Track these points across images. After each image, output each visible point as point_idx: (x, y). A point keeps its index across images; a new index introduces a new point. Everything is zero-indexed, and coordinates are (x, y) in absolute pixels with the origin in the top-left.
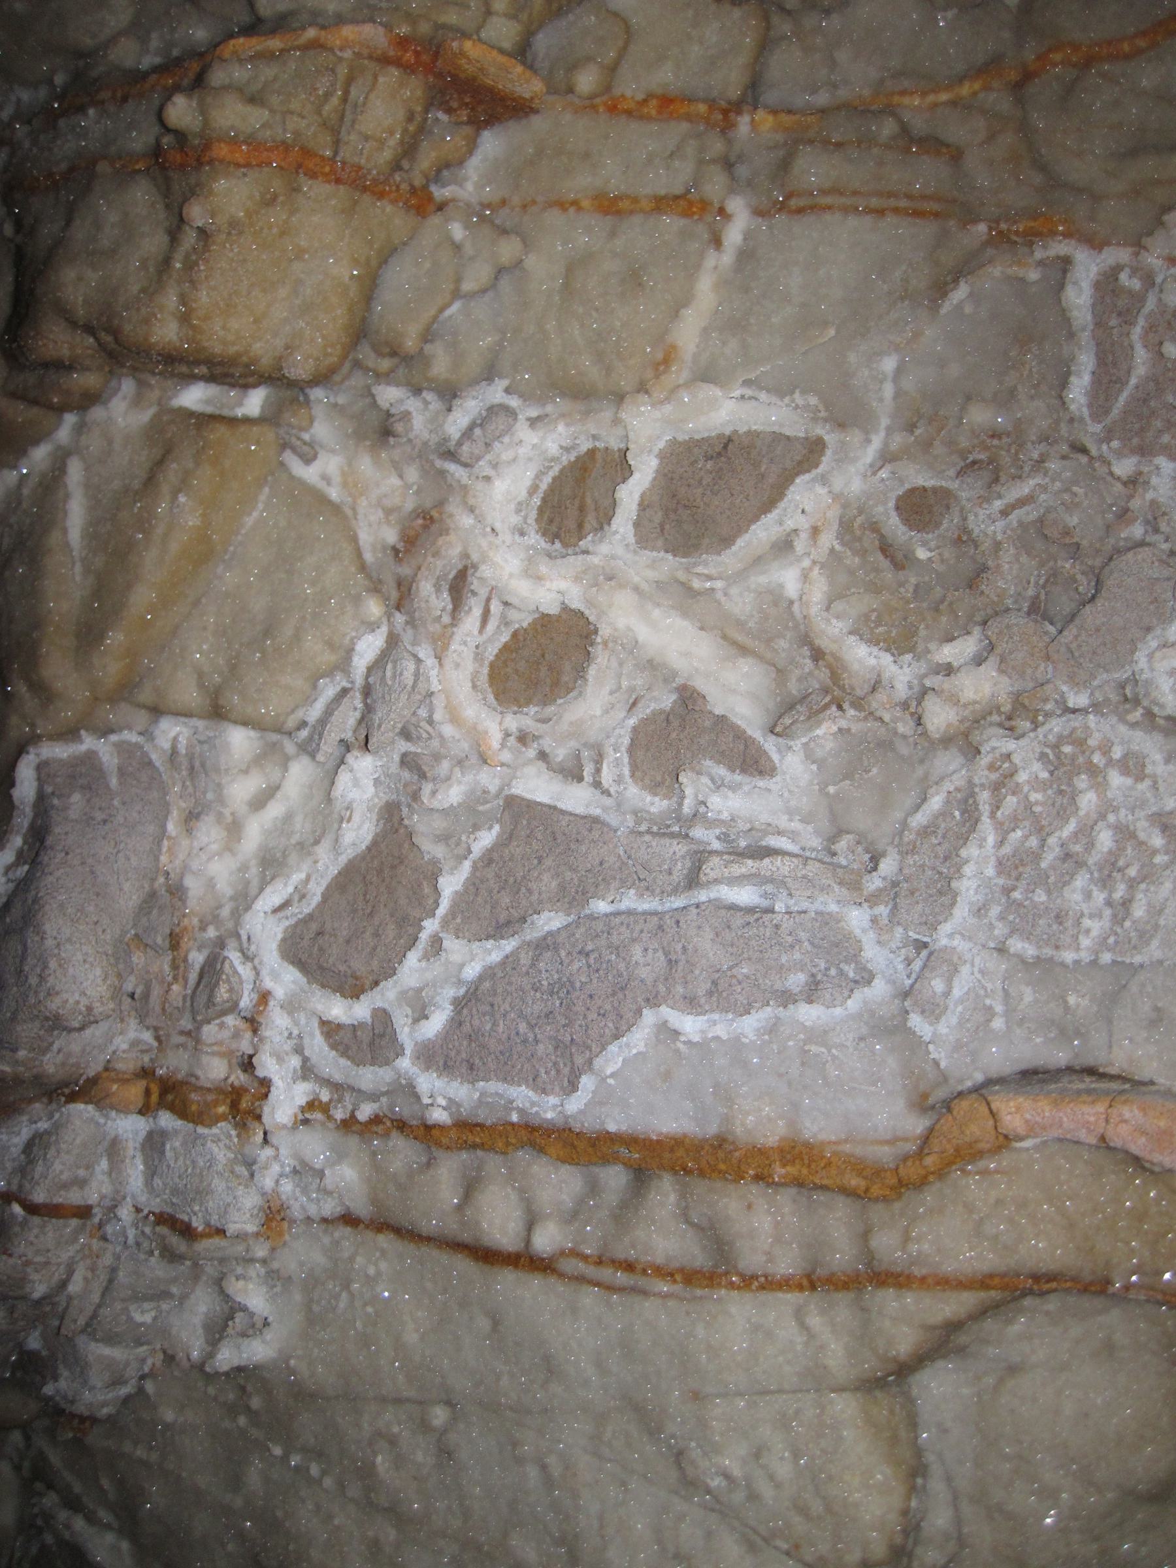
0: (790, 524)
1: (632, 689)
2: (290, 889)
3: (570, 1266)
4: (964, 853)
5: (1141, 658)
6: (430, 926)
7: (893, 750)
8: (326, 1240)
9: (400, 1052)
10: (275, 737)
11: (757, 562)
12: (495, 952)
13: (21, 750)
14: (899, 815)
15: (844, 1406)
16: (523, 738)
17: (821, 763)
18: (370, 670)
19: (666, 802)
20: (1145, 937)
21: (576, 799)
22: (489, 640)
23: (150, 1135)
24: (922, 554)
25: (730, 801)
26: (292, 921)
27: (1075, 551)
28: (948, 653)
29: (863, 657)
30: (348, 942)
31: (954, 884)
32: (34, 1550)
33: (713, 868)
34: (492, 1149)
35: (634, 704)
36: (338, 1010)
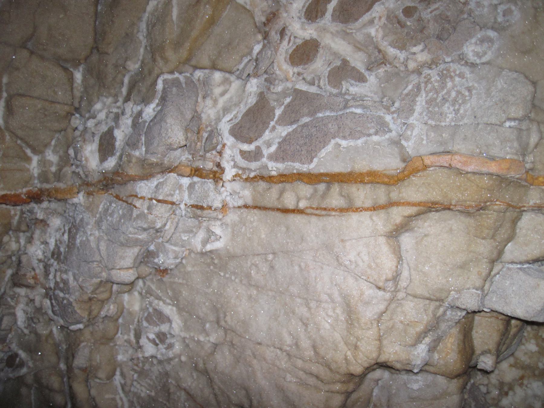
0: (374, 15)
1: (329, 60)
2: (232, 116)
3: (309, 211)
4: (417, 99)
5: (465, 48)
6: (272, 123)
7: (399, 75)
8: (239, 213)
9: (263, 156)
10: (227, 75)
11: (364, 26)
12: (290, 129)
13: (158, 76)
14: (400, 91)
15: (382, 240)
16: (299, 74)
17: (380, 79)
18: (258, 54)
19: (337, 91)
20: (463, 118)
21: (313, 89)
22: (290, 48)
23: (190, 184)
24: (409, 23)
25: (355, 89)
26: (232, 125)
27: (449, 22)
28: (415, 49)
29: (392, 51)
30: (249, 129)
31: (414, 107)
32: (146, 315)
33: (351, 103)
34: (288, 182)
35: (330, 64)
36: (246, 147)
